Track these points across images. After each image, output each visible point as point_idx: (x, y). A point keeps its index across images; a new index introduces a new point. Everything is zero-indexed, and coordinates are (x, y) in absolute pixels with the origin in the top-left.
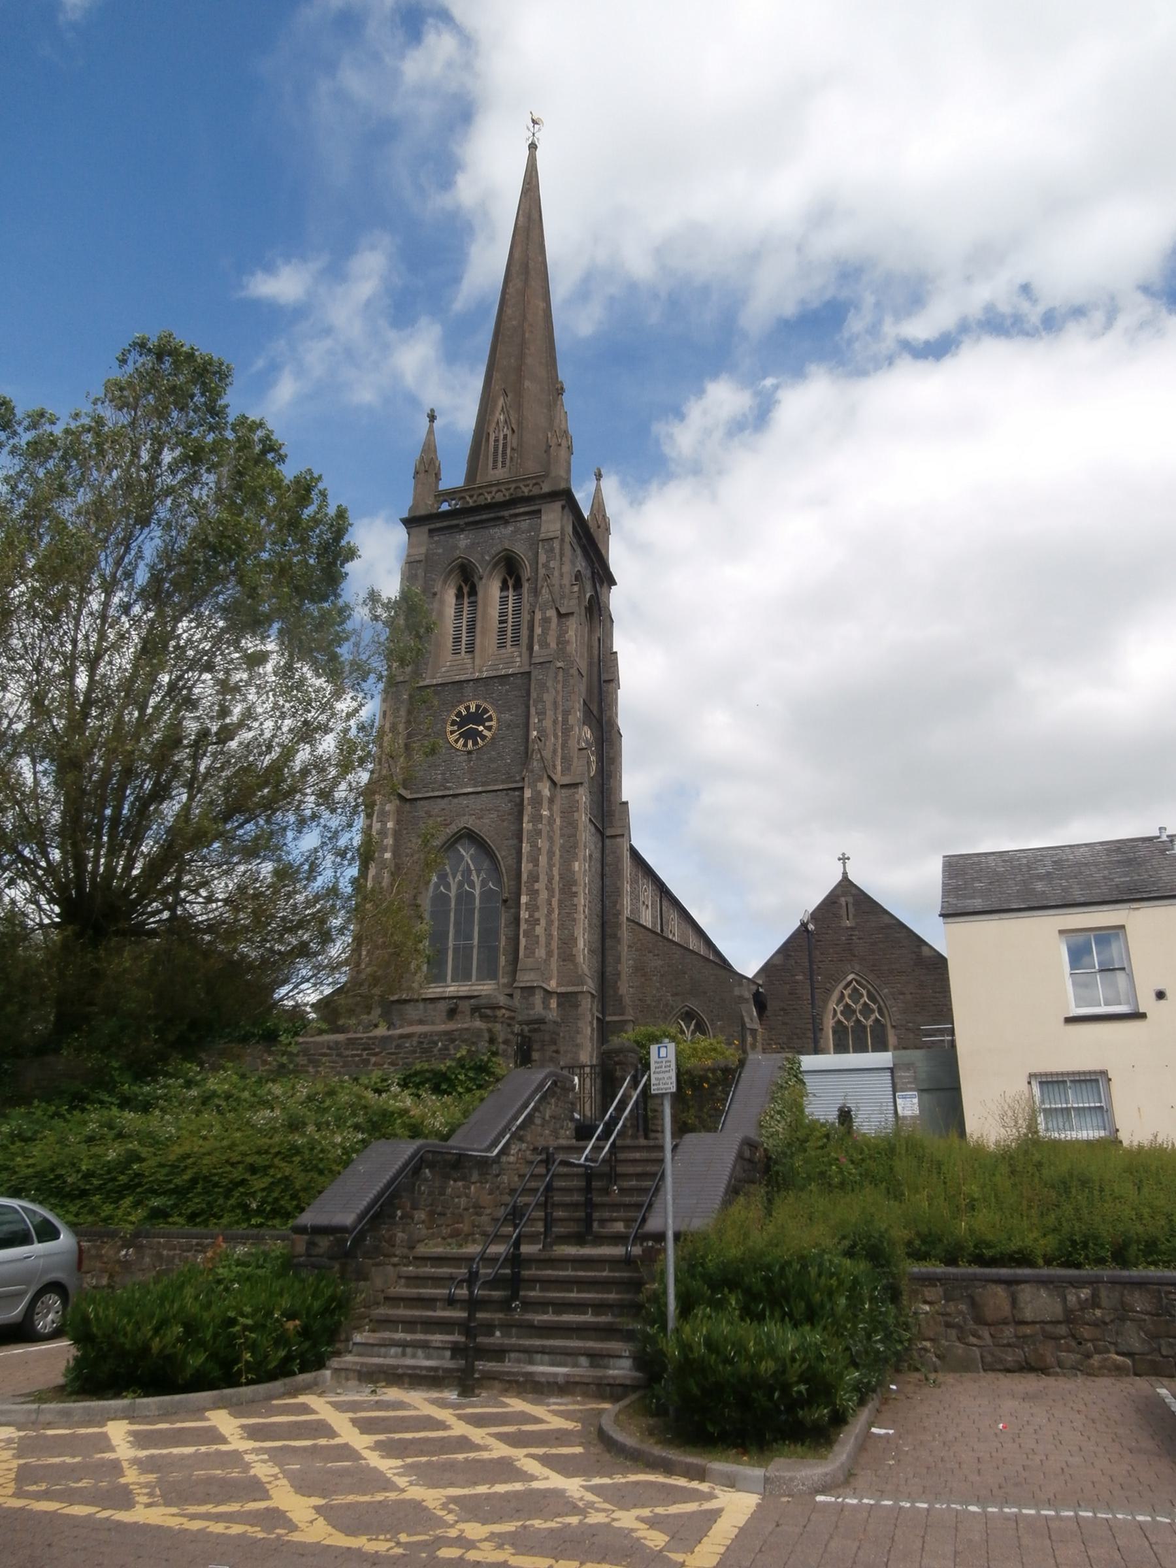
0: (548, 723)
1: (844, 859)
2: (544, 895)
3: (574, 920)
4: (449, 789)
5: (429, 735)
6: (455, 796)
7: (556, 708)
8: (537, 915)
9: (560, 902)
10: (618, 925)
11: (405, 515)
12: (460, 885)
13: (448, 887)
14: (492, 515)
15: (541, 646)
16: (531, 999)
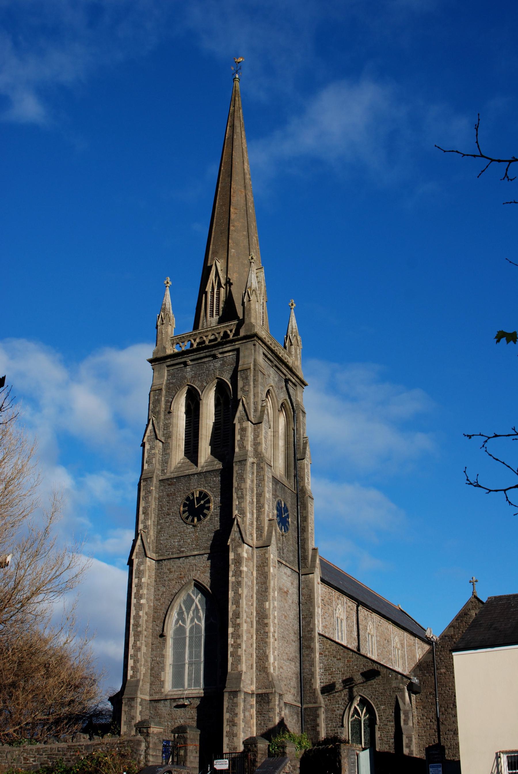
0: (149, 523)
1: (473, 583)
2: (245, 627)
3: (266, 643)
4: (183, 552)
5: (169, 514)
6: (187, 557)
7: (252, 492)
8: (239, 641)
9: (257, 630)
10: (312, 639)
11: (151, 357)
12: (192, 620)
13: (184, 621)
14: (193, 354)
15: (240, 448)
16: (235, 699)
